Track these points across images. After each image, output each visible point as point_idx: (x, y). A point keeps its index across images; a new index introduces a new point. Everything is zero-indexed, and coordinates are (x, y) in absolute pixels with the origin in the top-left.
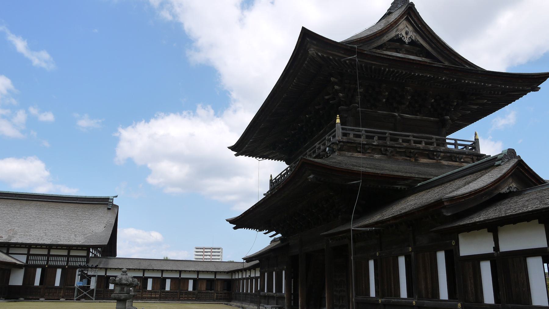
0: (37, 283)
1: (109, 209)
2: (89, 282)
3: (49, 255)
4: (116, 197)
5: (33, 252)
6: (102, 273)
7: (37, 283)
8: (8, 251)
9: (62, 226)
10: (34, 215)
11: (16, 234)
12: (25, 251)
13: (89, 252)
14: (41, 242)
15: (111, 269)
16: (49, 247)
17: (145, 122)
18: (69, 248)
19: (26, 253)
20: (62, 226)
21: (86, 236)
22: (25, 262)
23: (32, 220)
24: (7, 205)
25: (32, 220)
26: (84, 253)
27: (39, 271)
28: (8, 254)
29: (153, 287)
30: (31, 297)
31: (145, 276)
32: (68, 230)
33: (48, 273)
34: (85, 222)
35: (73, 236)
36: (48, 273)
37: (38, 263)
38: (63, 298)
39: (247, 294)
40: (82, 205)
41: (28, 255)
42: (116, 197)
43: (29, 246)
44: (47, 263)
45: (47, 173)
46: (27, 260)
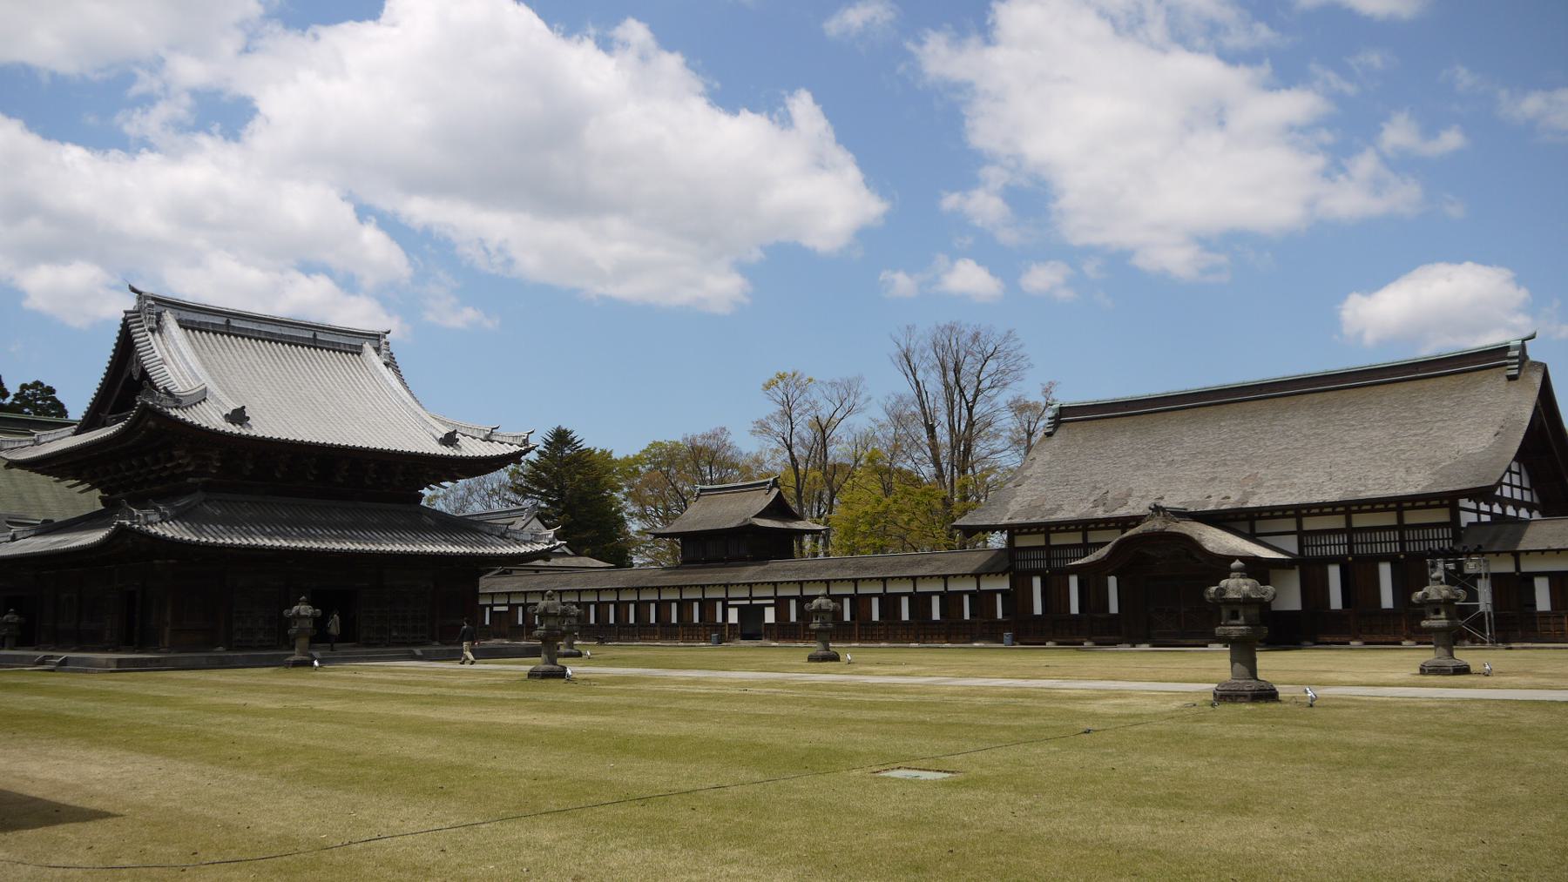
0: (1336, 602)
1: (1511, 378)
2: (1473, 596)
3: (1401, 527)
4: (1533, 337)
5: (1310, 524)
6: (1507, 567)
7: (1336, 602)
8: (1252, 528)
9: (1376, 450)
10: (1305, 431)
11: (1259, 485)
12: (1291, 525)
13: (1455, 511)
14: (1317, 498)
15: (1527, 552)
16: (1347, 508)
17: (1296, 134)
18: (1398, 504)
19: (1294, 528)
20: (1376, 450)
21: (1437, 468)
22: (1295, 550)
23: (1298, 445)
24: (1243, 417)
25: (1298, 445)
26: (1442, 516)
27: (1334, 572)
28: (1252, 537)
29: (1004, 614)
30: (1328, 639)
31: (1524, 569)
32: (1388, 459)
33: (1359, 576)
34: (1440, 429)
35: (1401, 473)
36: (1359, 576)
37: (1329, 551)
38: (1408, 638)
39: (722, 626)
40: (1431, 382)
41: (1301, 534)
42: (1533, 337)
43: (1299, 512)
44: (1403, 547)
45: (1523, 294)
46: (1301, 546)
